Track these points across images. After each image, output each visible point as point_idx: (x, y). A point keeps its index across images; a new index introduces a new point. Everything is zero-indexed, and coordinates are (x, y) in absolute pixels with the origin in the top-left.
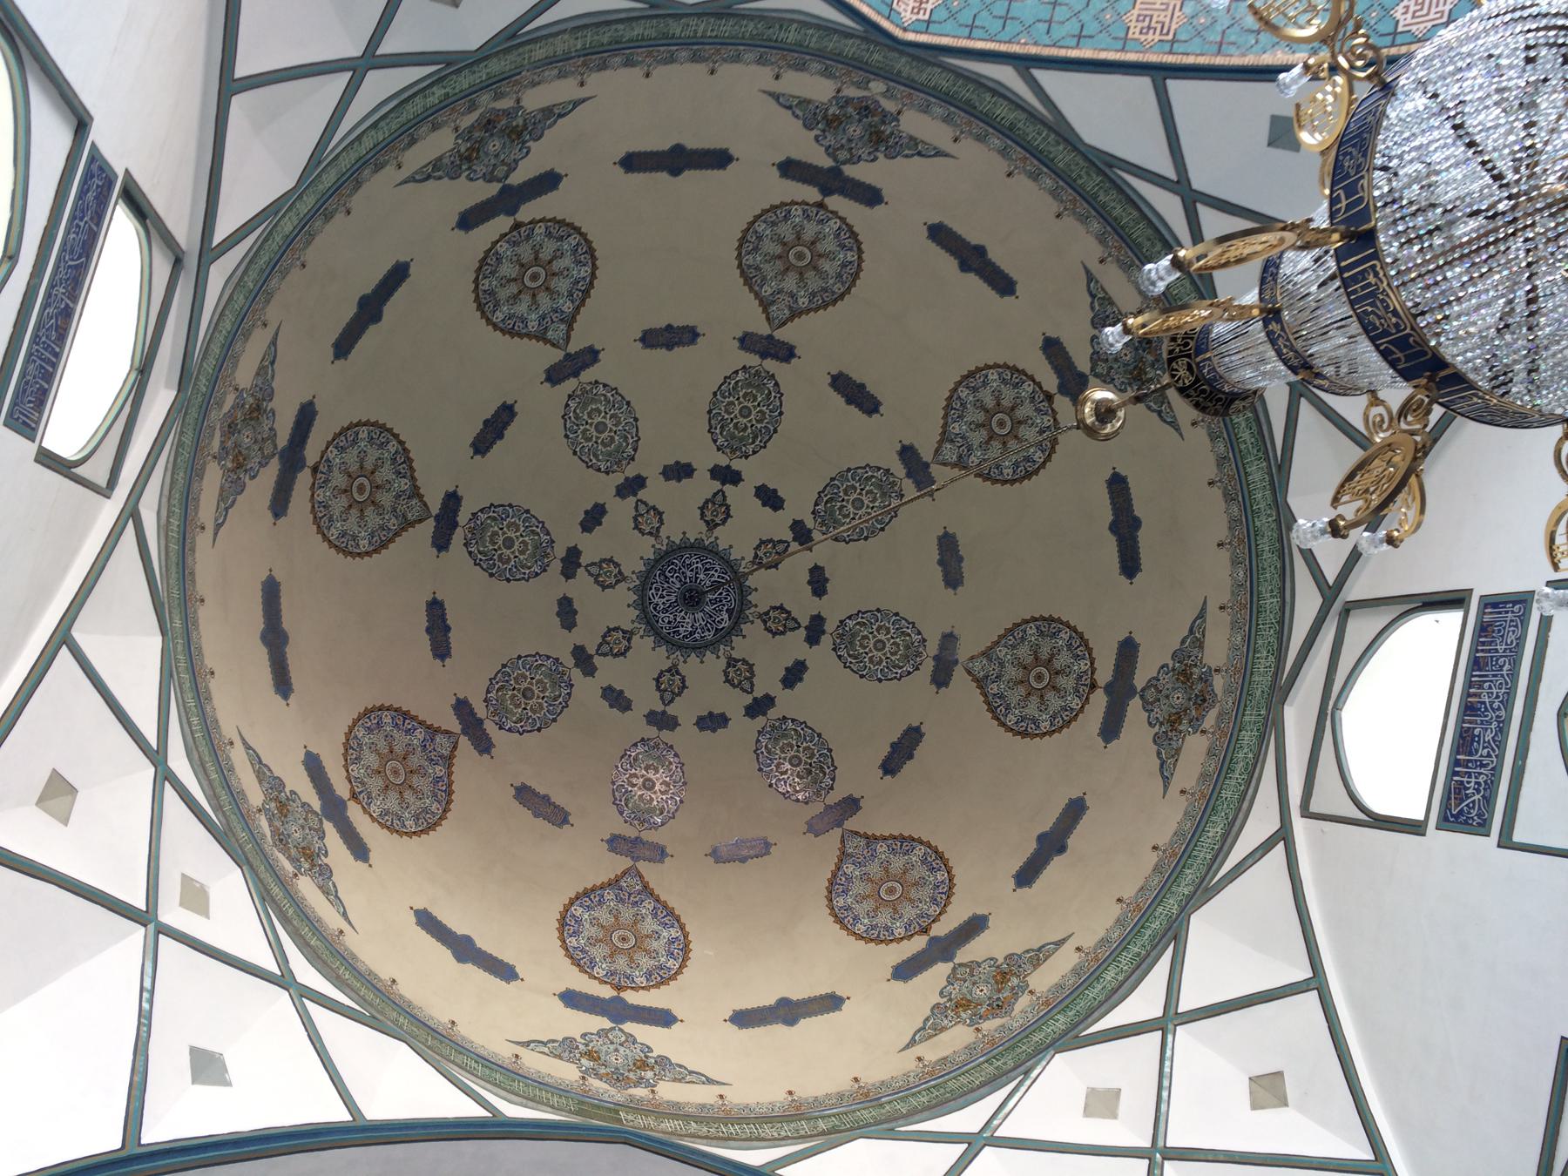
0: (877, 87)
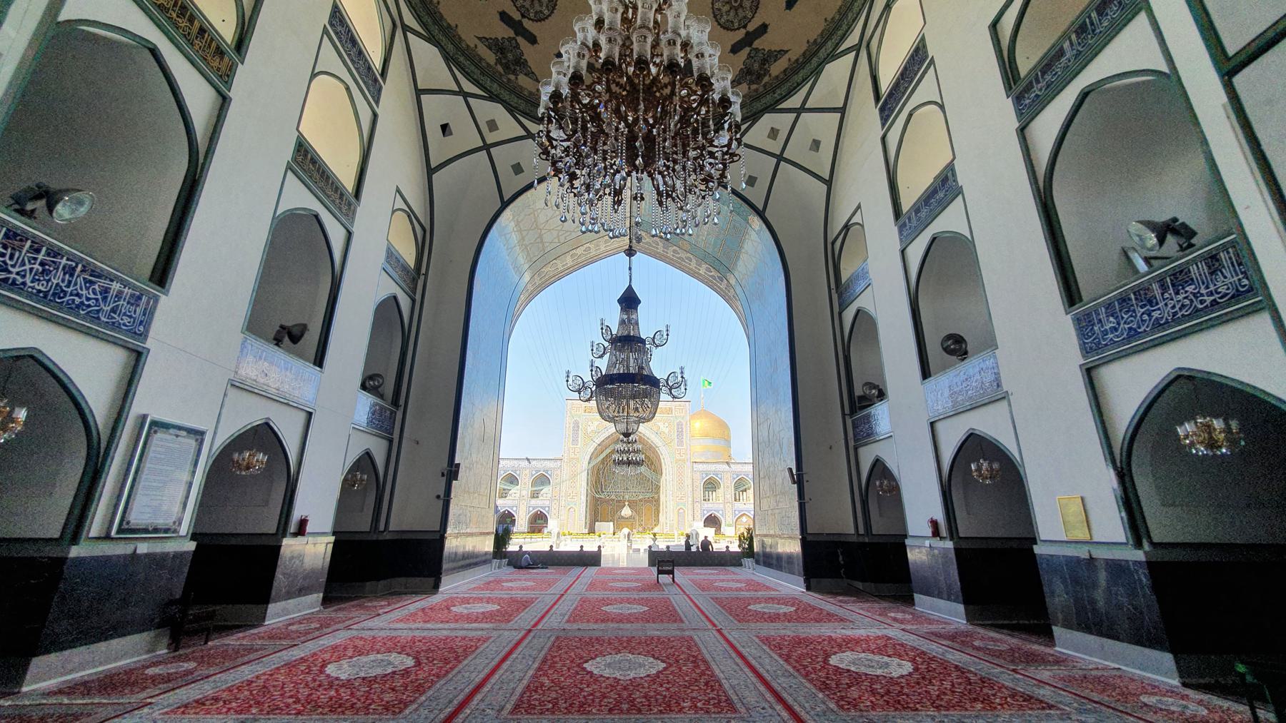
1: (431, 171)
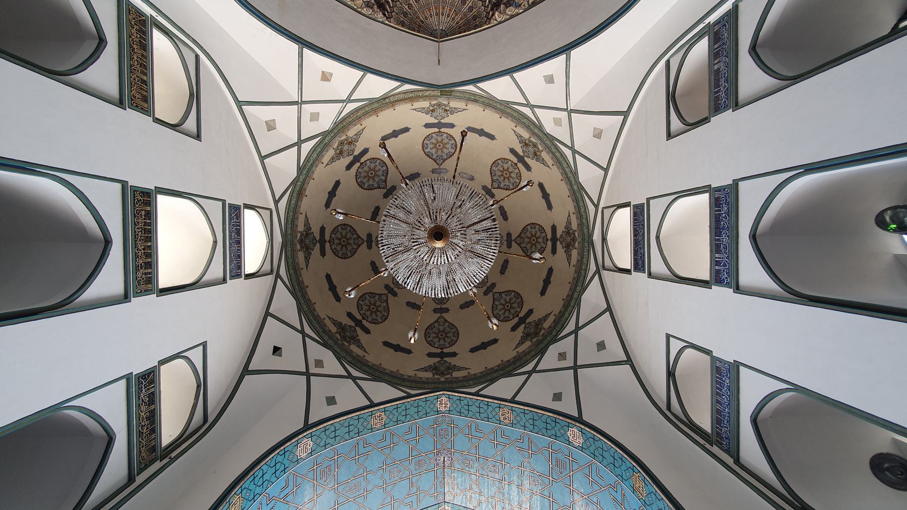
0: (443, 379)
1: (246, 371)
